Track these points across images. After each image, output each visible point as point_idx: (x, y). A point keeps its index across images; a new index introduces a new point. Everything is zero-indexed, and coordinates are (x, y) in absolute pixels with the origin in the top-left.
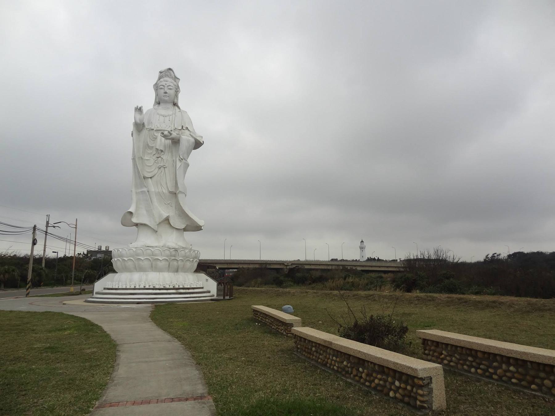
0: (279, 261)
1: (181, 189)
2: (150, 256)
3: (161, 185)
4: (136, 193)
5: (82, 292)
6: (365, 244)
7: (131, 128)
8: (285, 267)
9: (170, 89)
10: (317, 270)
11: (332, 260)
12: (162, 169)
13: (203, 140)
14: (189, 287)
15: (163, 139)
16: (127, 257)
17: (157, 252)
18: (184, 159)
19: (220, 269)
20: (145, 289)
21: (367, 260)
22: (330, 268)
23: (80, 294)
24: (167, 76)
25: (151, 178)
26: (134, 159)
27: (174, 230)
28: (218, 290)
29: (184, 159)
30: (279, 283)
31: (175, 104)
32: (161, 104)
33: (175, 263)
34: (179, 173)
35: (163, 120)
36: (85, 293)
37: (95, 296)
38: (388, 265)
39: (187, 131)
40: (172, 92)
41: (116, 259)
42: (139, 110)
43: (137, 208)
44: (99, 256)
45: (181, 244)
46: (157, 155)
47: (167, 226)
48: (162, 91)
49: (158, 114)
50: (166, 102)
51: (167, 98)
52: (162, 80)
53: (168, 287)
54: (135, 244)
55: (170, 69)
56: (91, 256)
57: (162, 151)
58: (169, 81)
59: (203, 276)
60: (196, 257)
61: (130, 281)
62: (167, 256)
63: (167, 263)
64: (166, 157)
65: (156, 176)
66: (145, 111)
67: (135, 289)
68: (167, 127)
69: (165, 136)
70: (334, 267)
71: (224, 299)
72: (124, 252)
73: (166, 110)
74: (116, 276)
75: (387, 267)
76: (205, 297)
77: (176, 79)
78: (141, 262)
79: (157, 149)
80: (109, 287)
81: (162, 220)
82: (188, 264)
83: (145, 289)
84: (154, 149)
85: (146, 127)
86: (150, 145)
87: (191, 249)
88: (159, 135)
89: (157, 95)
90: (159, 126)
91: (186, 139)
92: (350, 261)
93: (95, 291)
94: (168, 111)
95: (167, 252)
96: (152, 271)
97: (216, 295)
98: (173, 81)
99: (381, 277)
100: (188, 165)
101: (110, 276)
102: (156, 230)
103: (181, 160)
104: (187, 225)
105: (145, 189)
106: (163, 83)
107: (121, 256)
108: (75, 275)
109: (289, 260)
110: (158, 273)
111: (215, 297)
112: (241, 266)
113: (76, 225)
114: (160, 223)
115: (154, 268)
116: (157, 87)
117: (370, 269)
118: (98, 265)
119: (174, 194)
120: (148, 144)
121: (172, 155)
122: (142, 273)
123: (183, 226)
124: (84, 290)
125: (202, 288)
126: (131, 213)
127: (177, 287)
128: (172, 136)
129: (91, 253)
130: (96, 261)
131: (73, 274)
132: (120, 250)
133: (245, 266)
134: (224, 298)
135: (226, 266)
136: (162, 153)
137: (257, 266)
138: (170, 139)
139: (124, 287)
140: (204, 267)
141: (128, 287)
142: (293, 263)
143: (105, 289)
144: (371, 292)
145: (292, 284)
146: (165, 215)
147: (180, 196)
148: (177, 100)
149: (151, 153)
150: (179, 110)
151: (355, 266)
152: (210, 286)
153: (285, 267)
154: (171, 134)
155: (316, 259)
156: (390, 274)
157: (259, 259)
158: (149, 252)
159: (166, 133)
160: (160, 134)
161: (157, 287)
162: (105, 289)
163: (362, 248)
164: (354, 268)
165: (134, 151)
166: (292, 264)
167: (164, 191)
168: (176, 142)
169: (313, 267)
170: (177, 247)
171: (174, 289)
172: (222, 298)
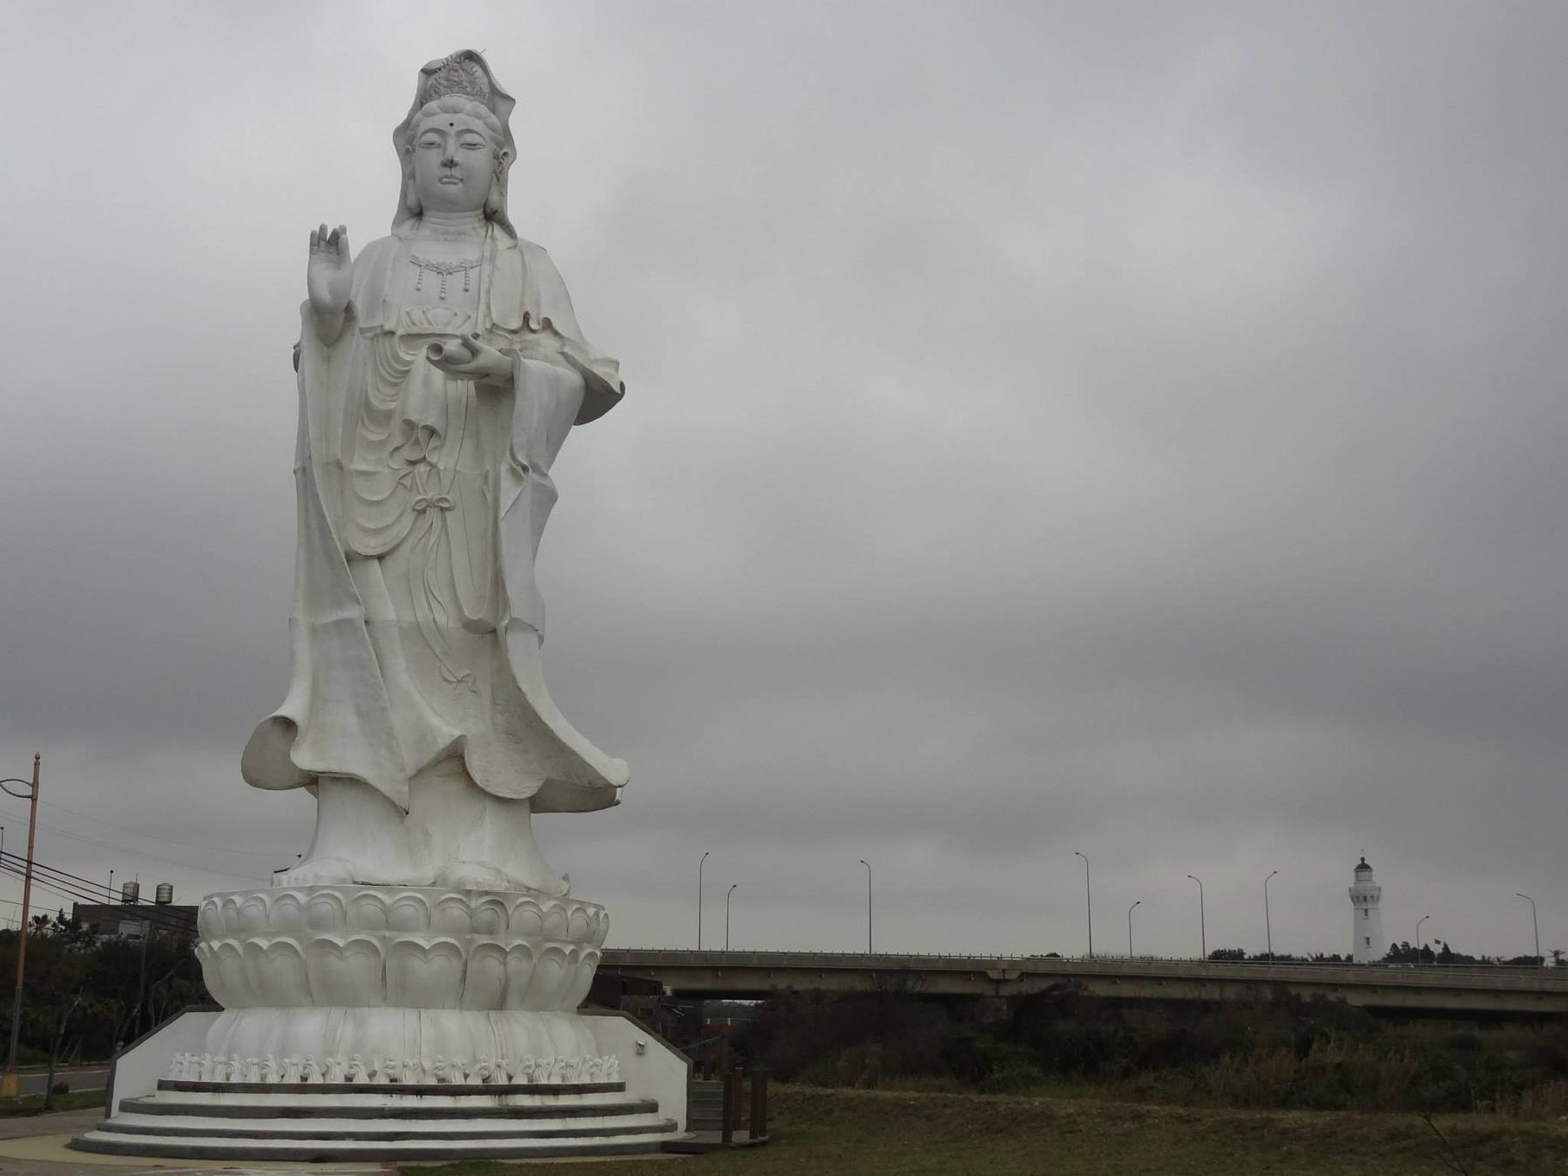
0: (960, 961)
1: (519, 607)
2: (372, 927)
3: (428, 591)
4: (314, 631)
5: (55, 1101)
6: (1379, 877)
7: (292, 328)
8: (989, 991)
9: (471, 146)
10: (1148, 1003)
11: (1218, 956)
12: (433, 516)
13: (624, 375)
14: (556, 1081)
15: (438, 375)
16: (266, 935)
17: (408, 911)
18: (537, 469)
19: (679, 994)
20: (350, 1088)
21: (1388, 959)
22: (1210, 993)
23: (49, 1108)
24: (455, 86)
25: (380, 558)
26: (303, 472)
27: (490, 809)
28: (695, 1098)
29: (537, 469)
30: (970, 1067)
31: (493, 216)
32: (430, 217)
33: (493, 964)
34: (513, 533)
35: (440, 288)
36: (69, 1107)
37: (119, 1118)
38: (1500, 982)
39: (545, 339)
40: (480, 160)
41: (216, 945)
42: (329, 244)
43: (317, 701)
44: (127, 929)
45: (519, 871)
46: (409, 453)
47: (456, 786)
48: (435, 157)
49: (415, 262)
50: (450, 206)
51: (454, 190)
52: (432, 105)
53: (458, 1080)
54: (303, 874)
55: (471, 56)
56: (95, 929)
57: (432, 432)
58: (467, 110)
59: (621, 1029)
60: (590, 937)
61: (283, 1051)
62: (456, 931)
63: (456, 964)
64: (449, 458)
65: (404, 551)
66: (355, 245)
67: (303, 1088)
68: (453, 320)
69: (447, 363)
70: (1231, 993)
71: (726, 1145)
72: (254, 911)
73: (454, 247)
74: (217, 1025)
75: (1497, 993)
76: (634, 1131)
77: (498, 99)
78: (333, 961)
79: (410, 425)
80: (185, 1078)
81: (429, 756)
82: (554, 970)
83: (350, 1088)
84: (396, 423)
85: (362, 322)
86: (375, 403)
87: (565, 899)
88: (418, 357)
89: (409, 176)
90: (417, 315)
91: (543, 374)
92: (1303, 962)
93: (121, 1092)
94: (468, 246)
95: (456, 911)
96: (386, 1001)
97: (682, 1124)
98: (484, 110)
99: (1468, 1044)
100: (550, 497)
101: (188, 1022)
102: (402, 800)
103: (521, 472)
104: (548, 783)
105: (353, 613)
106: (440, 121)
107: (242, 928)
108: (22, 1016)
109: (1006, 955)
110: (411, 1015)
111: (680, 1135)
112: (781, 983)
113: (35, 785)
114: (420, 772)
115: (393, 988)
116: (411, 140)
117: (1412, 1001)
118: (136, 969)
119: (488, 635)
120: (368, 406)
121: (478, 448)
122: (336, 1013)
123: (528, 788)
124: (62, 1090)
125: (620, 1087)
126: (288, 725)
127: (502, 1081)
128: (481, 361)
129: (89, 918)
130: (118, 953)
131: (16, 1011)
132: (238, 900)
133: (801, 984)
134: (727, 1137)
135: (706, 984)
136: (434, 443)
137: (860, 985)
138: (469, 374)
139: (254, 1079)
140: (622, 986)
141: (273, 1079)
142: (1029, 970)
143: (163, 1085)
144: (1482, 1122)
145: (1034, 1070)
146: (445, 730)
147: (517, 646)
148: (503, 194)
149: (383, 443)
150: (509, 242)
151: (1334, 986)
152: (661, 1077)
153: (989, 991)
154: (475, 352)
155: (1137, 953)
156: (1511, 1031)
157: (860, 948)
158: (370, 908)
159: (452, 346)
160: (424, 352)
161: (409, 1080)
162: (163, 1085)
163: (1363, 900)
164: (1332, 997)
165: (303, 434)
166: (1024, 976)
167: (441, 619)
168: (496, 388)
169: (1127, 991)
170: (501, 886)
171: (486, 1090)
172: (716, 1137)
